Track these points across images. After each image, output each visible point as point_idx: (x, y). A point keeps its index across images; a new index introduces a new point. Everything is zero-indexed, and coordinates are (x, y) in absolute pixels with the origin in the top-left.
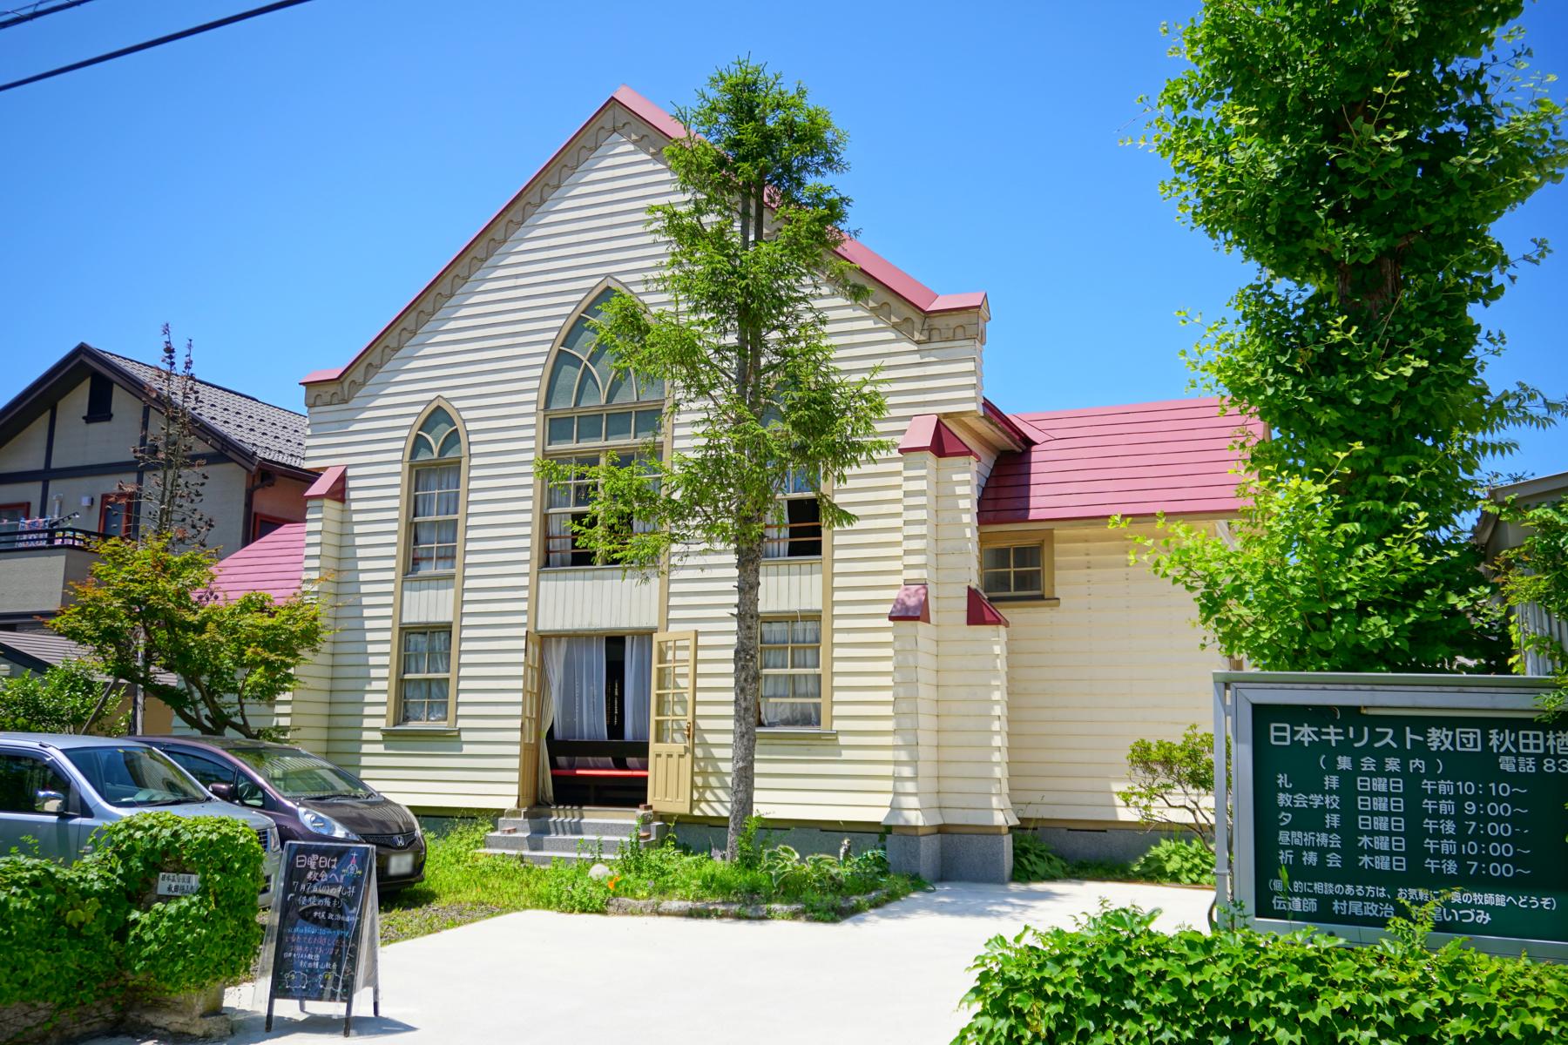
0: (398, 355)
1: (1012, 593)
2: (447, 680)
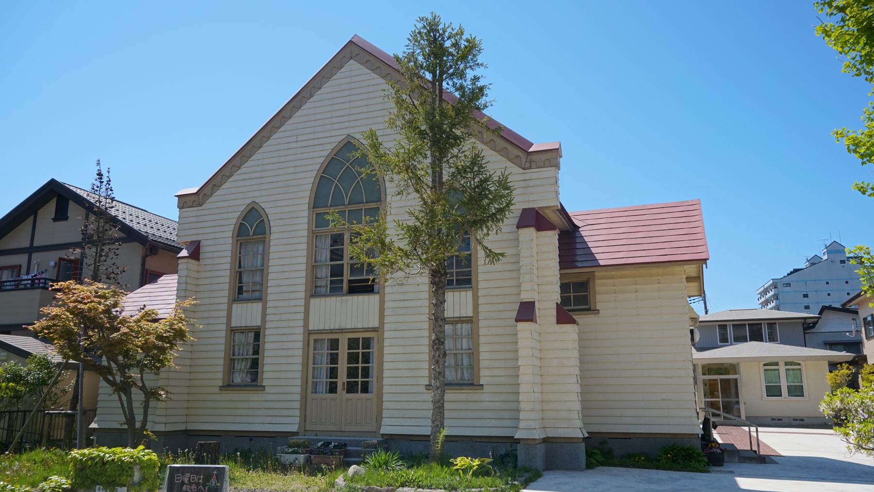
0: (231, 179)
1: (572, 307)
2: (704, 374)
